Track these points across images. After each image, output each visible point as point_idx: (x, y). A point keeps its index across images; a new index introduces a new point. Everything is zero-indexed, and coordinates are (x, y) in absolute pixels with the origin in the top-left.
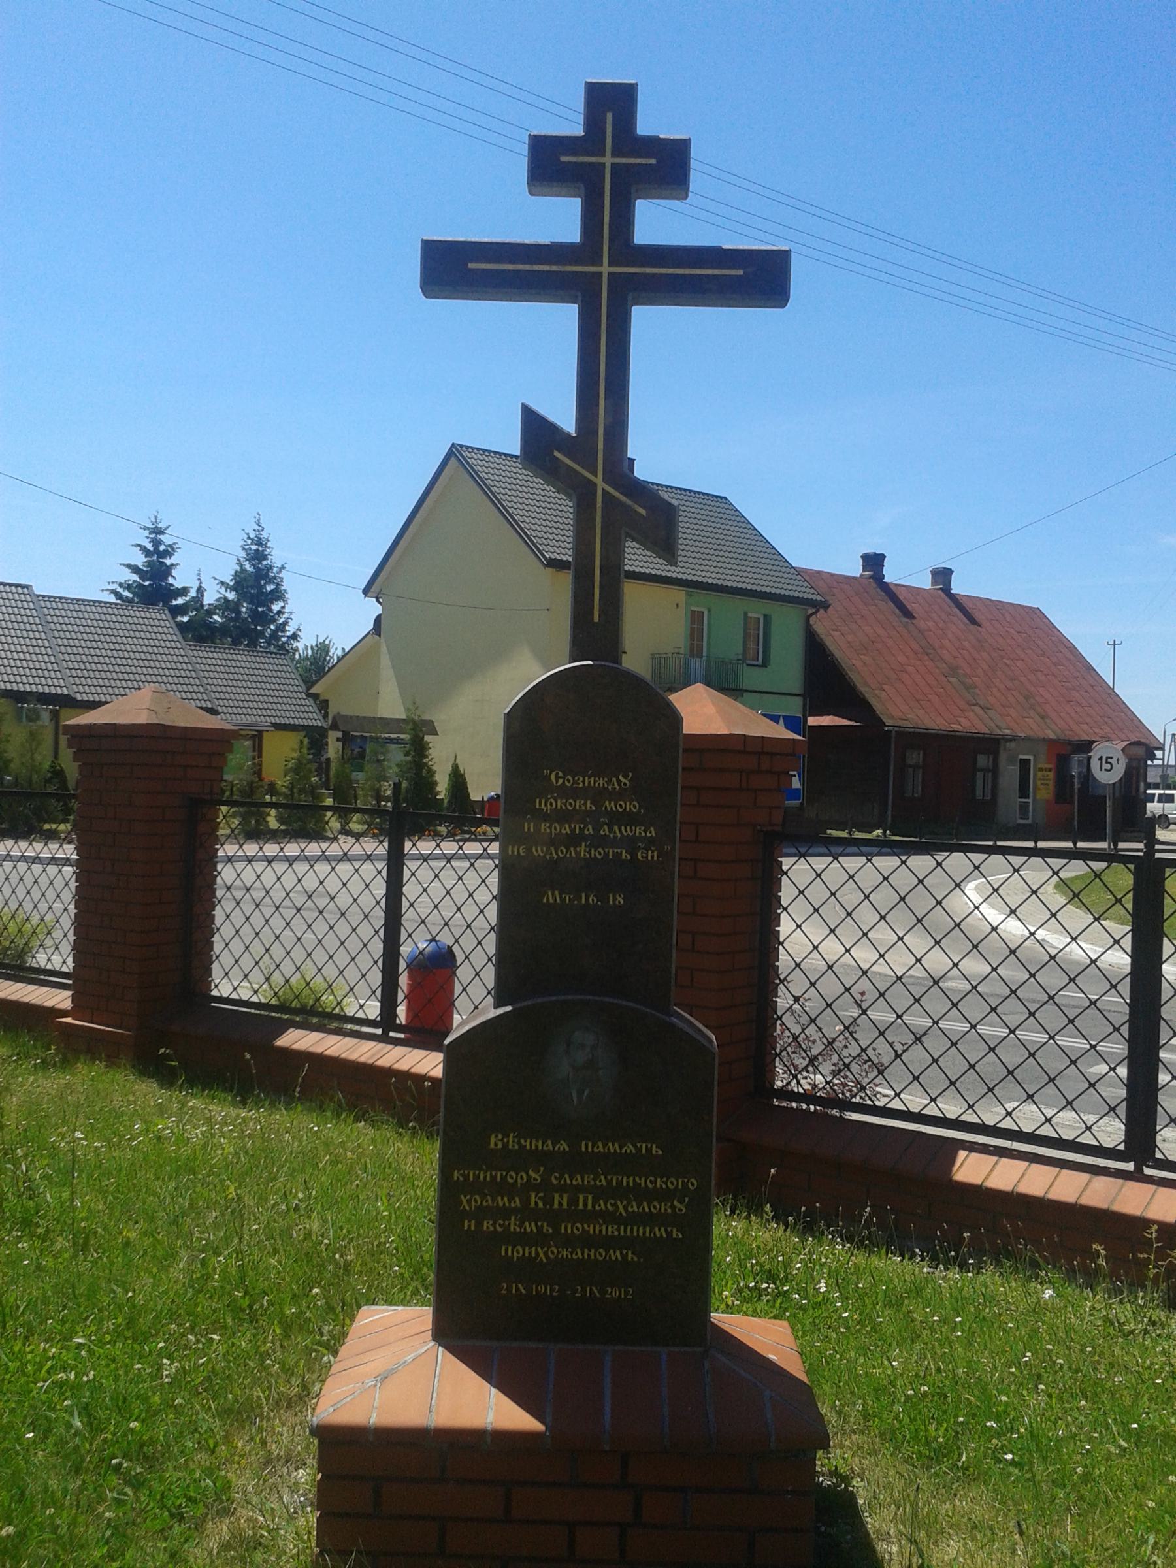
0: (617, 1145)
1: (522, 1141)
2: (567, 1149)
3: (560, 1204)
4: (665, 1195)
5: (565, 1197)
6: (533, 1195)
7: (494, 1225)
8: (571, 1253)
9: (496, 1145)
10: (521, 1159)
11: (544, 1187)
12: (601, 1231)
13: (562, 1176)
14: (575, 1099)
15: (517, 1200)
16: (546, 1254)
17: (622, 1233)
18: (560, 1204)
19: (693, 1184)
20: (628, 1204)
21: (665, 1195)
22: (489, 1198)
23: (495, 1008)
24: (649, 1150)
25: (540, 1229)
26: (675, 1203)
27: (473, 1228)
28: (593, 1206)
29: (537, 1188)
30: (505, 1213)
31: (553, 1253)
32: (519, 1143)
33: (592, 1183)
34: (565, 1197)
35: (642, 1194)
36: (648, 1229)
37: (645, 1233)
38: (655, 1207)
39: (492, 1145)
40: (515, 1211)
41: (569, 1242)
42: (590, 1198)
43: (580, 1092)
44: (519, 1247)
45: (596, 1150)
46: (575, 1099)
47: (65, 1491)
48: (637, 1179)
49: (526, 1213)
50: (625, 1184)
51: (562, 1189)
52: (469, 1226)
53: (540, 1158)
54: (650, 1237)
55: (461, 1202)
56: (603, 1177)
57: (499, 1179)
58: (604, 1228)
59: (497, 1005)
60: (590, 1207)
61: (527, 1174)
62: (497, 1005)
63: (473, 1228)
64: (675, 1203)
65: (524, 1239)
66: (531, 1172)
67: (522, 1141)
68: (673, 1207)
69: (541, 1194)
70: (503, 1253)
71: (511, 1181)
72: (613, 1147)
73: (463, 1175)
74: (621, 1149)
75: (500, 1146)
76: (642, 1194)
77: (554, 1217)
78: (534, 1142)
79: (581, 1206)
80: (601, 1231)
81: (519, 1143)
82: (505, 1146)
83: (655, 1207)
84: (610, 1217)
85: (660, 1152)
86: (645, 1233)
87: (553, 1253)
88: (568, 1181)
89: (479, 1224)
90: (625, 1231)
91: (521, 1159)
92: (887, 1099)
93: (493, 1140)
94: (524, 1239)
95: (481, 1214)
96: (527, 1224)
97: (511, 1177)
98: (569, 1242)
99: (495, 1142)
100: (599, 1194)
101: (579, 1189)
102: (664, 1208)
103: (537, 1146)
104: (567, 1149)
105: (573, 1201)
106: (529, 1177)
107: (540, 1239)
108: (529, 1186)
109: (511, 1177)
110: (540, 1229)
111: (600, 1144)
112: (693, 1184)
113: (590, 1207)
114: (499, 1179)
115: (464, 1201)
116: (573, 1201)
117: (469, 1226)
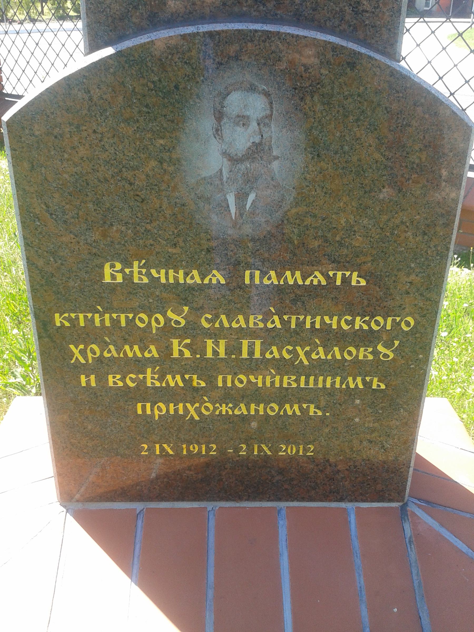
0: (298, 274)
1: (153, 272)
2: (223, 281)
3: (215, 353)
4: (367, 338)
5: (222, 343)
6: (175, 342)
7: (123, 379)
8: (233, 409)
9: (113, 277)
10: (155, 298)
11: (192, 331)
12: (273, 383)
13: (217, 316)
14: (233, 209)
15: (153, 348)
16: (197, 410)
17: (302, 385)
18: (215, 353)
19: (408, 324)
20: (311, 351)
21: (367, 338)
22: (112, 347)
23: (86, 54)
24: (345, 280)
25: (187, 382)
26: (380, 348)
27: (93, 384)
28: (263, 354)
29: (181, 333)
30: (139, 365)
31: (207, 409)
32: (148, 274)
33: (261, 325)
34: (222, 343)
35: (330, 337)
36: (338, 379)
37: (333, 383)
38: (350, 353)
39: (108, 279)
40: (152, 362)
41: (229, 396)
42: (258, 343)
43: (241, 197)
44: (161, 405)
45: (266, 282)
46: (233, 209)
47: (261, 87)
48: (327, 319)
49: (166, 363)
50: (308, 326)
51: (215, 335)
52: (88, 382)
53: (184, 295)
54: (340, 390)
55: (73, 354)
56: (276, 318)
57: (123, 324)
58: (277, 378)
59: (93, 46)
60: (257, 355)
61: (164, 315)
62: (93, 46)
63: (93, 384)
64: (380, 348)
65: (167, 395)
66: (170, 314)
67: (153, 272)
68: (375, 353)
69: (188, 341)
70: (140, 412)
71: (142, 325)
72: (292, 278)
73: (69, 319)
74: (304, 279)
75: (120, 279)
76: (330, 337)
77: (207, 368)
78: (171, 272)
79: (245, 355)
80: (273, 383)
81: (148, 274)
82: (128, 278)
83: (350, 353)
84: (282, 367)
85: (363, 283)
86: (333, 383)
87: (207, 409)
88: (226, 325)
89: (102, 379)
90: (307, 383)
91: (155, 298)
92: (420, 21)
93: (107, 270)
94: (167, 395)
95: (102, 366)
96: (169, 377)
97: (141, 320)
98: (229, 396)
99: (111, 273)
100: (270, 337)
101: (243, 333)
102: (363, 354)
103: (176, 278)
104: (223, 281)
105: (234, 349)
106: (168, 320)
107: (190, 394)
108: (169, 331)
109: (141, 320)
110: (187, 382)
111: (273, 273)
112: (408, 324)
113: (257, 355)
114: (123, 324)
115: (76, 351)
116: (234, 349)
117: (88, 382)
